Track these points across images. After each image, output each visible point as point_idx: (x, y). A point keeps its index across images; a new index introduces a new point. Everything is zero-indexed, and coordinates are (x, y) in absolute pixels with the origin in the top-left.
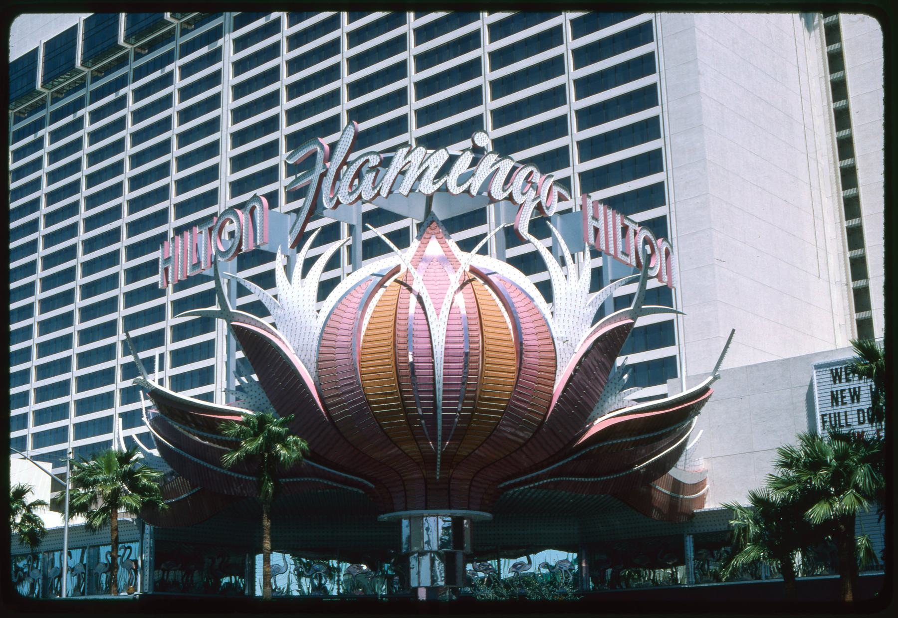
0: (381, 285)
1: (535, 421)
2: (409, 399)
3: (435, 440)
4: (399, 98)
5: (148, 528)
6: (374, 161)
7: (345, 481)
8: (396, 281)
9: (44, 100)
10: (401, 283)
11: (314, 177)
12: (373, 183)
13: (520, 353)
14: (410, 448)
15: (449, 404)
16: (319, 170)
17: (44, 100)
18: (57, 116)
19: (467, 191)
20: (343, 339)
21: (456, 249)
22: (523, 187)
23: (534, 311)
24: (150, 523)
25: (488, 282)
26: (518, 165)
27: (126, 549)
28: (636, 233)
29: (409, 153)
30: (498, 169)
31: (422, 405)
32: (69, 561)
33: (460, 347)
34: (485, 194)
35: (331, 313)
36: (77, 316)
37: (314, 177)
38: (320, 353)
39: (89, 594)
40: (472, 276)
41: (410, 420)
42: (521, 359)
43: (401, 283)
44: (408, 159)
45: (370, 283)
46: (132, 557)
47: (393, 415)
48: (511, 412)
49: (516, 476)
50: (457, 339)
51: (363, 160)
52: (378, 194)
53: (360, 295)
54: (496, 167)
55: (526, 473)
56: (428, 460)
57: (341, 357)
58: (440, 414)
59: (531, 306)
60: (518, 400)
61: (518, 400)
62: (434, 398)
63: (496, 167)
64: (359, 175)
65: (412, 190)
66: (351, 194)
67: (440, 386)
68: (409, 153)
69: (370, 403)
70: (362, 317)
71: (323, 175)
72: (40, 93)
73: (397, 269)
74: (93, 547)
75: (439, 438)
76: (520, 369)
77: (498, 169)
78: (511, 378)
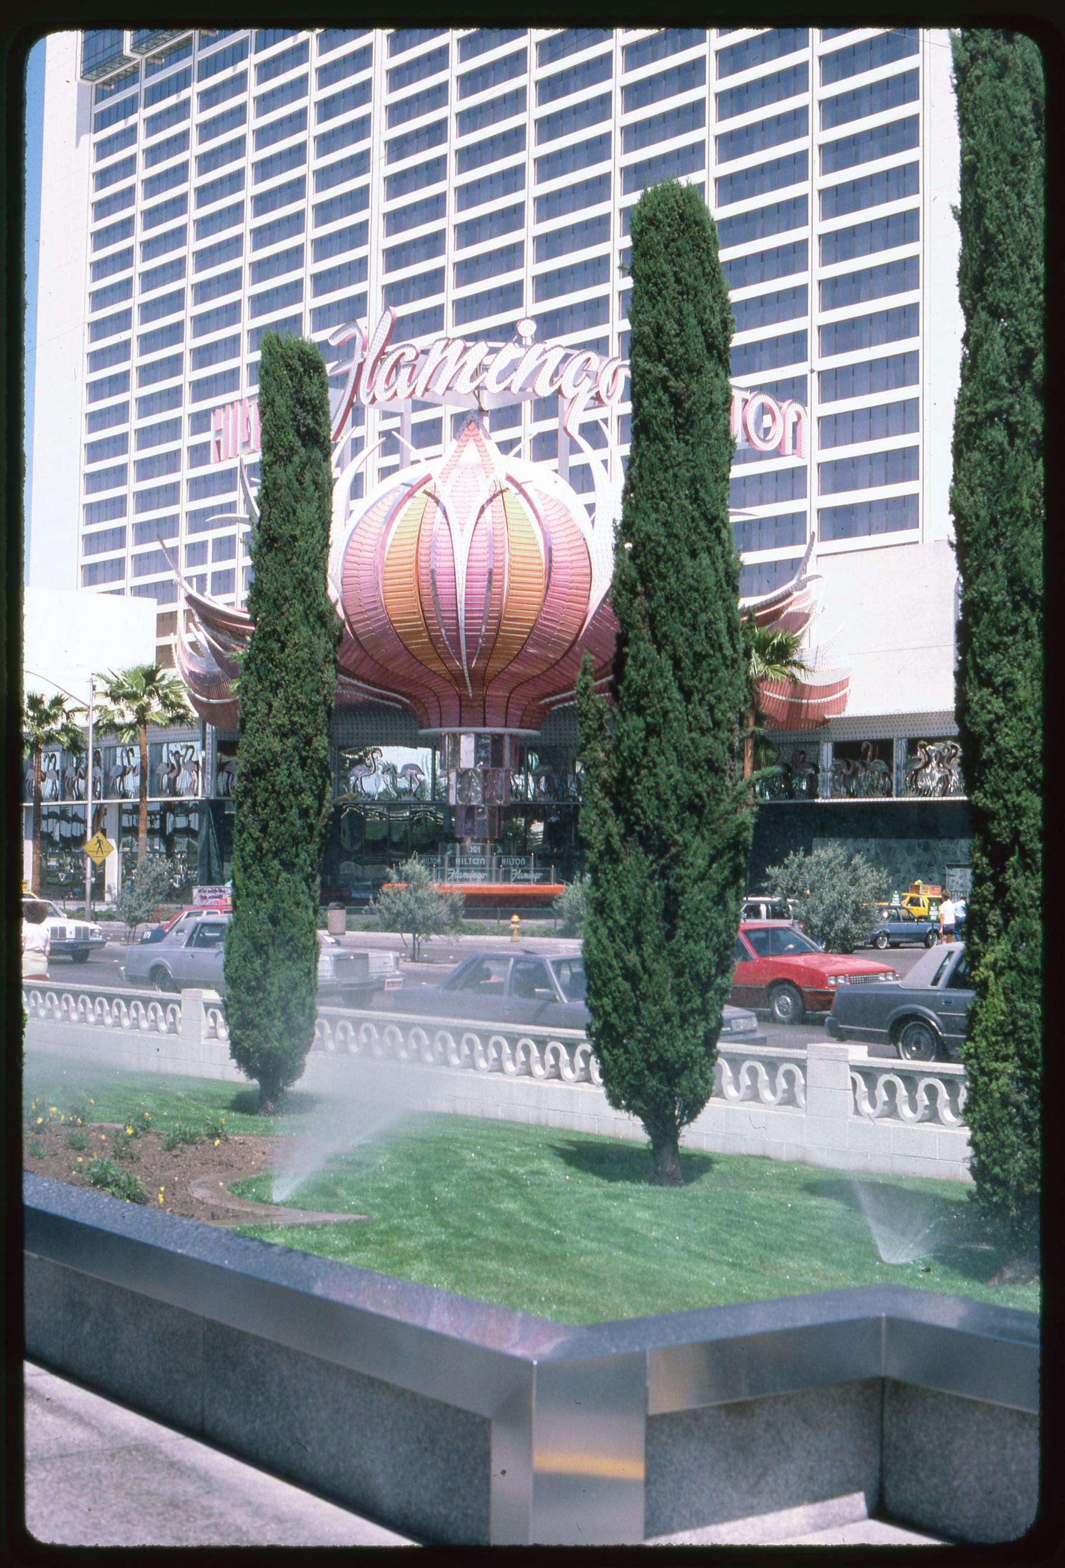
0: (410, 495)
1: (566, 641)
2: (432, 618)
3: (460, 659)
4: (600, 107)
5: (209, 728)
6: (410, 354)
7: (382, 697)
8: (425, 492)
9: (135, 70)
10: (429, 494)
11: (352, 366)
12: (409, 380)
13: (549, 571)
14: (435, 667)
15: (472, 624)
16: (358, 359)
17: (135, 70)
18: (155, 94)
19: (508, 388)
20: (367, 556)
21: (494, 451)
22: (577, 376)
23: (570, 524)
24: (212, 724)
25: (522, 491)
26: (570, 351)
27: (188, 748)
28: (746, 401)
29: (447, 345)
30: (545, 362)
31: (446, 625)
32: (97, 769)
33: (483, 566)
34: (530, 390)
35: (357, 526)
36: (310, 218)
37: (352, 366)
38: (345, 569)
39: (63, 799)
40: (507, 484)
41: (434, 641)
42: (550, 576)
43: (429, 494)
44: (446, 353)
45: (397, 494)
46: (194, 759)
47: (416, 635)
48: (537, 635)
49: (555, 693)
50: (482, 557)
51: (399, 352)
52: (413, 392)
53: (385, 508)
54: (543, 358)
55: (563, 692)
56: (457, 678)
57: (365, 575)
58: (463, 634)
59: (565, 519)
60: (545, 619)
61: (545, 619)
62: (457, 618)
63: (543, 358)
64: (396, 365)
65: (448, 388)
66: (386, 390)
67: (461, 606)
68: (447, 345)
69: (392, 622)
70: (387, 532)
71: (360, 366)
72: (129, 59)
73: (428, 478)
74: (156, 744)
75: (464, 658)
76: (548, 587)
77: (545, 362)
78: (537, 597)
